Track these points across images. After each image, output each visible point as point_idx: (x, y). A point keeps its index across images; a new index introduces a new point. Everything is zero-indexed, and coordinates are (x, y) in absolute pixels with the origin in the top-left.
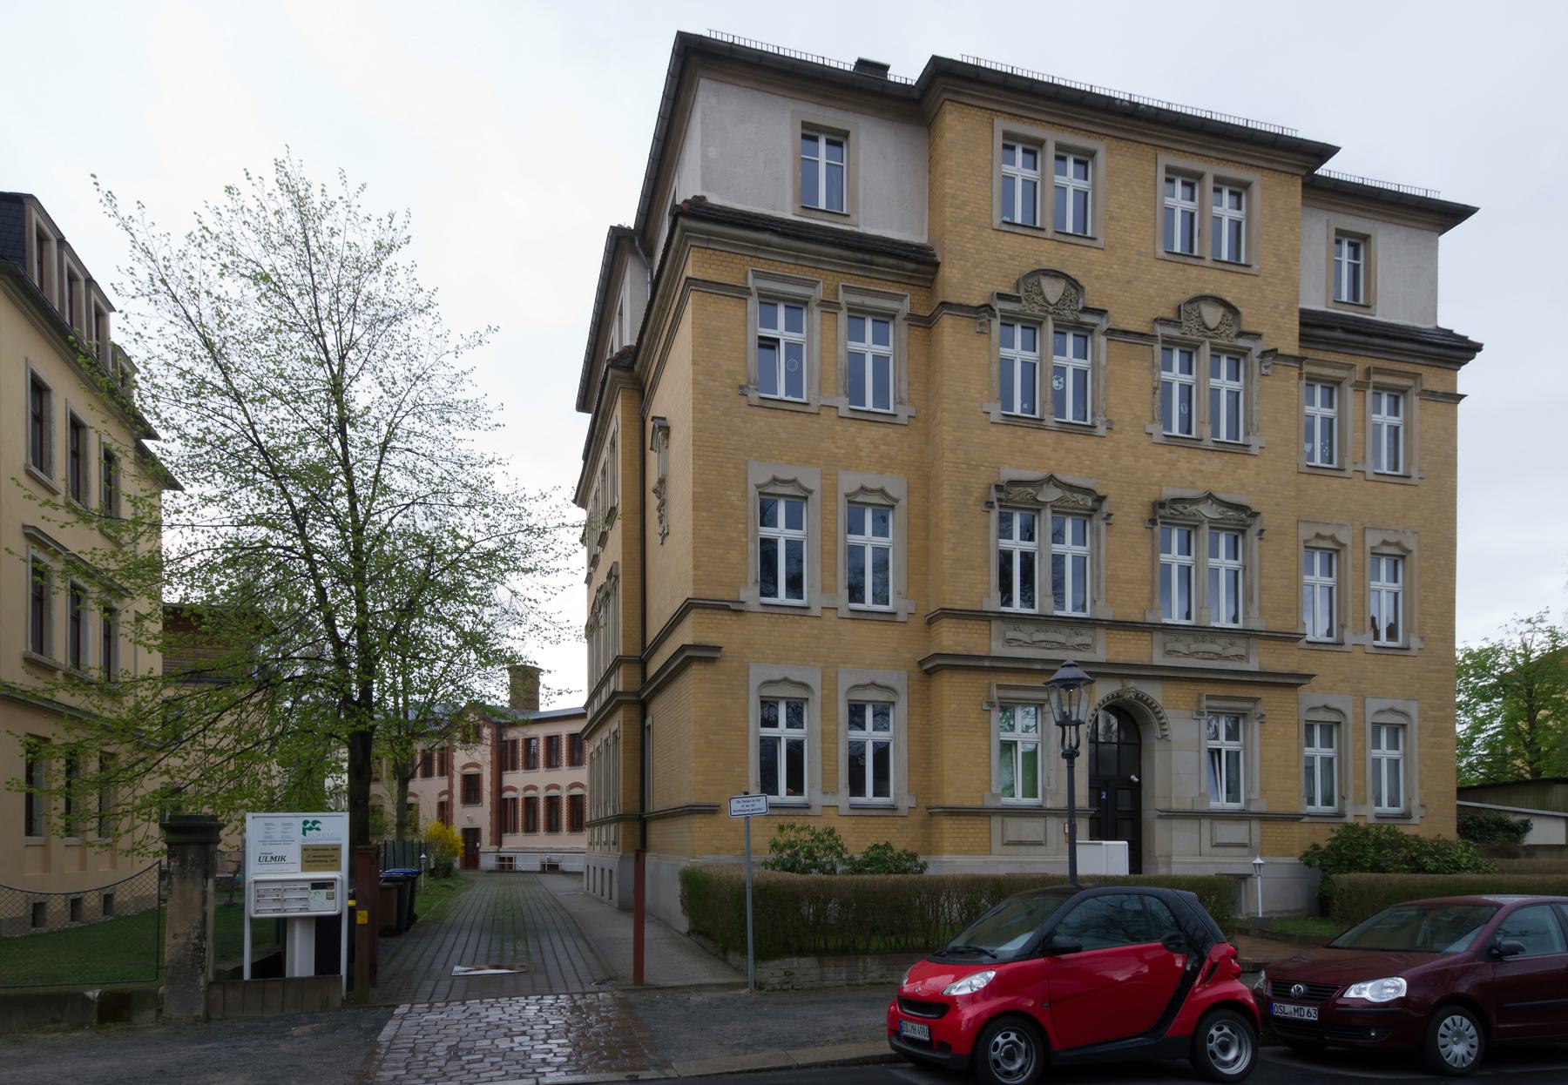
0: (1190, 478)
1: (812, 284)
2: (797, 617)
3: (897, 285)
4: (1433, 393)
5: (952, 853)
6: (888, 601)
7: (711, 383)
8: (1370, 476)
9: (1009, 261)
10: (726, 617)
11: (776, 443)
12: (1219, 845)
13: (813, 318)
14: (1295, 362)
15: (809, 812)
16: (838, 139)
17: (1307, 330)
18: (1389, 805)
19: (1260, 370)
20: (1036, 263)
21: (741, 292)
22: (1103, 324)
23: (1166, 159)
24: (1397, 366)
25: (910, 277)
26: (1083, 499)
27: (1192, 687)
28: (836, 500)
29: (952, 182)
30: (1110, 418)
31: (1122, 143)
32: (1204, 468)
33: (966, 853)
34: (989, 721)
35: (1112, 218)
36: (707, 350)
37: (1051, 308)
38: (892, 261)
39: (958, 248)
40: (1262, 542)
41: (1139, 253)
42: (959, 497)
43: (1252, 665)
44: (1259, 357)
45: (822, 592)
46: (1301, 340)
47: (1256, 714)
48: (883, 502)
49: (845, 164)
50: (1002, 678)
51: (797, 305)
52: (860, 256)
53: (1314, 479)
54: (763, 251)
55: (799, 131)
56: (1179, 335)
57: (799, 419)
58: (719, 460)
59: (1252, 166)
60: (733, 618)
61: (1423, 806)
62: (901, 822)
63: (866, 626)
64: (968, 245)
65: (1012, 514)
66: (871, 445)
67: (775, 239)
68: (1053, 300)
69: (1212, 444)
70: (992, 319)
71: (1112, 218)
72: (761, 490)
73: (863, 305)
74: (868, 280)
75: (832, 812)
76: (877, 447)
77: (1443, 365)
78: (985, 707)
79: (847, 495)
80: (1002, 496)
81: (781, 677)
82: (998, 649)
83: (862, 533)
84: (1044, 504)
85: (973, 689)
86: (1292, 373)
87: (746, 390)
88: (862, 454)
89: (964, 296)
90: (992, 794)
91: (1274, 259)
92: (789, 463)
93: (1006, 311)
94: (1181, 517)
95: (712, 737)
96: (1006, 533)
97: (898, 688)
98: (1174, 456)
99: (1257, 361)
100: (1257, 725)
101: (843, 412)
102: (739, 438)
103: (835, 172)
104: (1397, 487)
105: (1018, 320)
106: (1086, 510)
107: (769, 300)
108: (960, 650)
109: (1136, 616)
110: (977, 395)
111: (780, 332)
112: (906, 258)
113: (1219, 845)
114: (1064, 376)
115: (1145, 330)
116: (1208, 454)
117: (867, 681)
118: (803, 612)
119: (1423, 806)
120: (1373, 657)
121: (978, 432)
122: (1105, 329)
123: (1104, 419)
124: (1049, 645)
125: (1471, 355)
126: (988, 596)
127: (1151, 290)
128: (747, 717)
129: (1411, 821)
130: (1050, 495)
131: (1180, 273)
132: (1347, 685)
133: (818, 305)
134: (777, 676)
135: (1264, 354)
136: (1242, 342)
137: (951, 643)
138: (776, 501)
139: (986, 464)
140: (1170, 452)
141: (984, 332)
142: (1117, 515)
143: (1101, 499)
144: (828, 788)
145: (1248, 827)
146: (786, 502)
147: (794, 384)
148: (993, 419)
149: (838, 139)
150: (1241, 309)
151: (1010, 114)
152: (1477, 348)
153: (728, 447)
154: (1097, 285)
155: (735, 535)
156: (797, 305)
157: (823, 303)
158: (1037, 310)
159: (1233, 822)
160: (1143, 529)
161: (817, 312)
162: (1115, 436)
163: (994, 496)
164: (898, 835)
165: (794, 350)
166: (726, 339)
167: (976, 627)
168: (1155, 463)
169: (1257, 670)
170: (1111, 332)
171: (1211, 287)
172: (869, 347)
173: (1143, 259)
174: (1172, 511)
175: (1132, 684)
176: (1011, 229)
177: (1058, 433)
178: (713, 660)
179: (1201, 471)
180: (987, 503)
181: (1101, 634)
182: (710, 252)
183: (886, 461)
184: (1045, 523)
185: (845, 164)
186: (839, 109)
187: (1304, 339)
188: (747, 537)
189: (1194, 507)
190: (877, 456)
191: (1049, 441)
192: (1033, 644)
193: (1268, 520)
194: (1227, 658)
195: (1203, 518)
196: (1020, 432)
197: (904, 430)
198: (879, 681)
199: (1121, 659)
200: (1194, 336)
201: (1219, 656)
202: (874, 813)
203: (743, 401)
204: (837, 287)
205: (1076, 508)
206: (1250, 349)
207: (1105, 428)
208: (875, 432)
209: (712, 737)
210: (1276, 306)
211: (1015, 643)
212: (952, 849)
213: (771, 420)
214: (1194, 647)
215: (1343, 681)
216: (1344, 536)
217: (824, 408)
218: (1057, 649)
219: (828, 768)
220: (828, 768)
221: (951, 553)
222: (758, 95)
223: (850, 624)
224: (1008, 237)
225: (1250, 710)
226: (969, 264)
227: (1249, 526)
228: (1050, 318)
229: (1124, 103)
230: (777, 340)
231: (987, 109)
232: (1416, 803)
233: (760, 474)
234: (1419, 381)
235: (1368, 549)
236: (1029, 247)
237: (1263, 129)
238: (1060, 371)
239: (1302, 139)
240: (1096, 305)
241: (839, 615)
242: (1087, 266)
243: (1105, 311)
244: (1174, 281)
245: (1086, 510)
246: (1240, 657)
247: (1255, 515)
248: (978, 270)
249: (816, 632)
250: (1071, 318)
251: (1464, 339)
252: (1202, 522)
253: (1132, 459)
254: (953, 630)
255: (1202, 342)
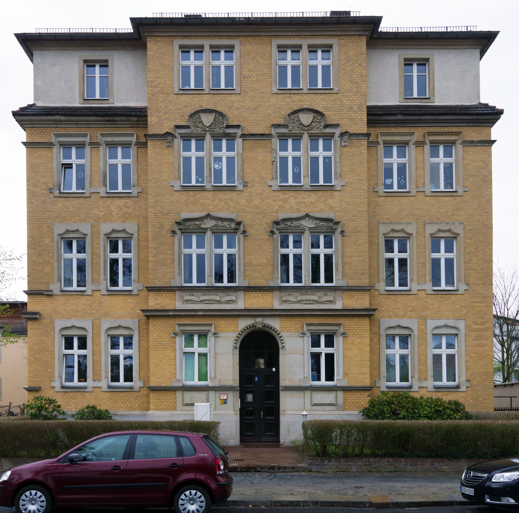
0: (297, 207)
1: (85, 136)
2: (79, 296)
3: (132, 129)
4: (472, 142)
5: (154, 410)
6: (454, 284)
7: (35, 189)
8: (428, 193)
9: (184, 109)
10: (43, 298)
11: (68, 213)
12: (315, 405)
13: (411, 150)
14: (364, 136)
15: (86, 390)
16: (104, 64)
17: (370, 118)
18: (401, 381)
19: (341, 144)
20: (200, 107)
21: (49, 145)
22: (239, 132)
23: (276, 42)
24: (442, 130)
25: (138, 124)
26: (228, 224)
27: (299, 320)
28: (99, 237)
29: (151, 75)
30: (245, 180)
31: (250, 39)
32: (305, 200)
33: (162, 410)
34: (175, 343)
35: (245, 77)
36: (34, 174)
37: (207, 128)
38: (124, 118)
39: (155, 106)
40: (344, 238)
41: (263, 93)
42: (158, 230)
43: (339, 305)
44: (339, 137)
45: (92, 283)
46: (368, 123)
47: (340, 332)
48: (126, 236)
49: (427, 74)
50: (183, 320)
51: (80, 146)
52: (107, 118)
53: (390, 199)
54: (60, 124)
55: (403, 62)
56: (287, 132)
57: (80, 200)
58: (40, 224)
59: (332, 35)
60: (47, 298)
61: (468, 381)
62: (136, 394)
63: (116, 298)
64: (160, 104)
65: (288, 235)
66: (118, 209)
67: (62, 118)
68: (208, 125)
69: (309, 187)
70: (174, 139)
71: (245, 77)
72: (61, 236)
73: (113, 141)
74: (116, 129)
75: (98, 390)
76: (121, 209)
77: (479, 125)
78: (173, 335)
79: (384, 234)
80: (182, 227)
81: (397, 325)
82: (179, 305)
83: (439, 252)
84: (206, 229)
85: (167, 327)
86: (363, 143)
87: (52, 190)
88: (113, 214)
89: (159, 129)
90: (177, 380)
91: (349, 83)
92: (75, 222)
93: (182, 134)
94: (291, 228)
95: (36, 355)
96: (284, 244)
97: (133, 327)
98: (286, 196)
99: (338, 139)
100: (341, 338)
101: (103, 194)
102: (49, 213)
103: (422, 80)
104: (448, 198)
105: (193, 137)
106: (231, 230)
107: (66, 146)
108: (159, 307)
109: (263, 283)
110: (166, 178)
111: (74, 160)
112: (130, 116)
113: (315, 405)
114: (221, 161)
115: (267, 132)
116: (308, 193)
117: (116, 325)
118: (82, 293)
119: (468, 381)
120: (433, 296)
121: (168, 196)
122: (240, 135)
123: (242, 181)
124: (210, 302)
125: (496, 117)
126: (174, 278)
127: (269, 111)
128: (54, 345)
129: (460, 390)
130: (209, 224)
131: (288, 99)
132: (414, 313)
133: (89, 145)
134: (69, 324)
135: (342, 135)
136: (328, 130)
137: (153, 304)
138: (440, 240)
139: (172, 212)
140: (283, 194)
141: (170, 145)
142: (249, 230)
143: (239, 223)
144: (423, 378)
145: (303, 394)
146: (445, 240)
147: (81, 184)
148: (175, 189)
149: (104, 64)
150: (324, 113)
151: (182, 36)
152: (501, 112)
153: (44, 218)
154: (236, 113)
155: (47, 259)
156: (80, 146)
157: (91, 144)
158: (199, 130)
159: (324, 392)
160: (267, 237)
161: (413, 147)
162: (249, 189)
163: (176, 228)
164: (134, 401)
165: (81, 168)
166: (43, 168)
167: (168, 295)
168: (275, 201)
169: (341, 308)
170: (243, 136)
171: (308, 103)
172: (120, 161)
173: (264, 95)
174: (284, 226)
175: (259, 320)
176: (185, 92)
177: (214, 192)
178: (36, 319)
179: (303, 202)
180: (172, 231)
181: (241, 294)
182: (35, 129)
183: (126, 216)
184: (306, 239)
185: (427, 74)
186: (103, 50)
187: (371, 123)
188: (53, 259)
189: (299, 222)
190: (122, 214)
191: (209, 196)
192: (201, 302)
193: (349, 225)
194: (322, 303)
195: (305, 228)
196: (192, 194)
197: (135, 199)
198: (123, 325)
199: (254, 307)
200: (296, 131)
201: (316, 302)
202: (120, 390)
203: (52, 196)
204: (378, 133)
205: (226, 230)
206: (334, 133)
207: (242, 186)
208: (120, 202)
209: (36, 355)
210: (351, 108)
211: (288, 302)
212: (154, 407)
213: (66, 203)
214: (299, 298)
215: (411, 311)
216: (411, 229)
217: (92, 194)
218: (215, 303)
219: (96, 368)
220: (96, 368)
221: (153, 259)
222: (61, 52)
223: (108, 298)
224: (183, 97)
225: (337, 330)
226: (161, 114)
227: (336, 229)
228: (208, 134)
229: (241, 19)
230: (72, 164)
231: (169, 36)
232: (464, 378)
233: (59, 229)
234: (461, 136)
235: (427, 235)
236: (196, 100)
237: (295, 16)
238: (218, 160)
239: (291, 18)
240: (236, 123)
241: (102, 294)
242: (230, 104)
243: (240, 126)
244: (285, 104)
245: (231, 230)
246: (331, 302)
247: (337, 223)
248: (166, 116)
249: (90, 302)
250: (220, 132)
251: (494, 108)
252: (305, 230)
253: (260, 200)
254: (155, 297)
255: (303, 134)
